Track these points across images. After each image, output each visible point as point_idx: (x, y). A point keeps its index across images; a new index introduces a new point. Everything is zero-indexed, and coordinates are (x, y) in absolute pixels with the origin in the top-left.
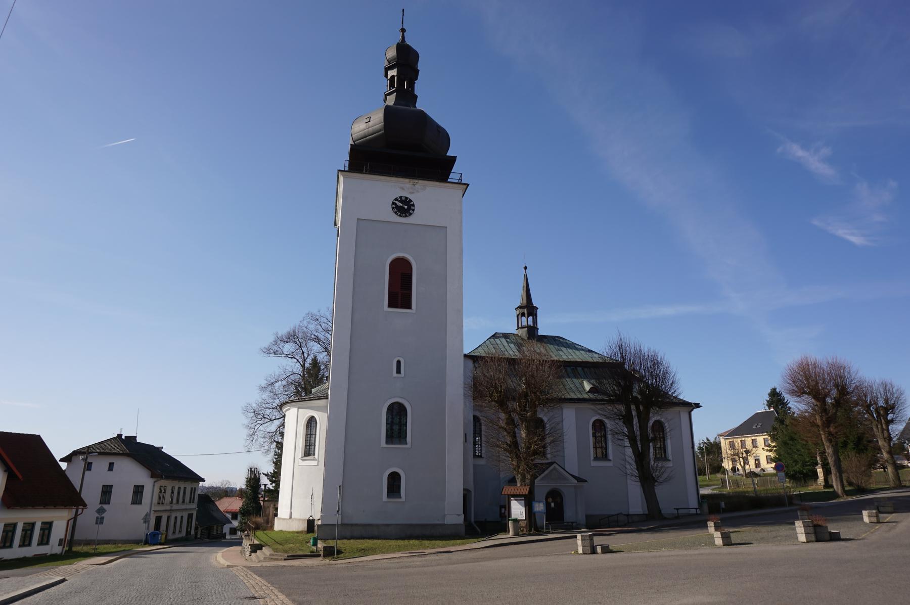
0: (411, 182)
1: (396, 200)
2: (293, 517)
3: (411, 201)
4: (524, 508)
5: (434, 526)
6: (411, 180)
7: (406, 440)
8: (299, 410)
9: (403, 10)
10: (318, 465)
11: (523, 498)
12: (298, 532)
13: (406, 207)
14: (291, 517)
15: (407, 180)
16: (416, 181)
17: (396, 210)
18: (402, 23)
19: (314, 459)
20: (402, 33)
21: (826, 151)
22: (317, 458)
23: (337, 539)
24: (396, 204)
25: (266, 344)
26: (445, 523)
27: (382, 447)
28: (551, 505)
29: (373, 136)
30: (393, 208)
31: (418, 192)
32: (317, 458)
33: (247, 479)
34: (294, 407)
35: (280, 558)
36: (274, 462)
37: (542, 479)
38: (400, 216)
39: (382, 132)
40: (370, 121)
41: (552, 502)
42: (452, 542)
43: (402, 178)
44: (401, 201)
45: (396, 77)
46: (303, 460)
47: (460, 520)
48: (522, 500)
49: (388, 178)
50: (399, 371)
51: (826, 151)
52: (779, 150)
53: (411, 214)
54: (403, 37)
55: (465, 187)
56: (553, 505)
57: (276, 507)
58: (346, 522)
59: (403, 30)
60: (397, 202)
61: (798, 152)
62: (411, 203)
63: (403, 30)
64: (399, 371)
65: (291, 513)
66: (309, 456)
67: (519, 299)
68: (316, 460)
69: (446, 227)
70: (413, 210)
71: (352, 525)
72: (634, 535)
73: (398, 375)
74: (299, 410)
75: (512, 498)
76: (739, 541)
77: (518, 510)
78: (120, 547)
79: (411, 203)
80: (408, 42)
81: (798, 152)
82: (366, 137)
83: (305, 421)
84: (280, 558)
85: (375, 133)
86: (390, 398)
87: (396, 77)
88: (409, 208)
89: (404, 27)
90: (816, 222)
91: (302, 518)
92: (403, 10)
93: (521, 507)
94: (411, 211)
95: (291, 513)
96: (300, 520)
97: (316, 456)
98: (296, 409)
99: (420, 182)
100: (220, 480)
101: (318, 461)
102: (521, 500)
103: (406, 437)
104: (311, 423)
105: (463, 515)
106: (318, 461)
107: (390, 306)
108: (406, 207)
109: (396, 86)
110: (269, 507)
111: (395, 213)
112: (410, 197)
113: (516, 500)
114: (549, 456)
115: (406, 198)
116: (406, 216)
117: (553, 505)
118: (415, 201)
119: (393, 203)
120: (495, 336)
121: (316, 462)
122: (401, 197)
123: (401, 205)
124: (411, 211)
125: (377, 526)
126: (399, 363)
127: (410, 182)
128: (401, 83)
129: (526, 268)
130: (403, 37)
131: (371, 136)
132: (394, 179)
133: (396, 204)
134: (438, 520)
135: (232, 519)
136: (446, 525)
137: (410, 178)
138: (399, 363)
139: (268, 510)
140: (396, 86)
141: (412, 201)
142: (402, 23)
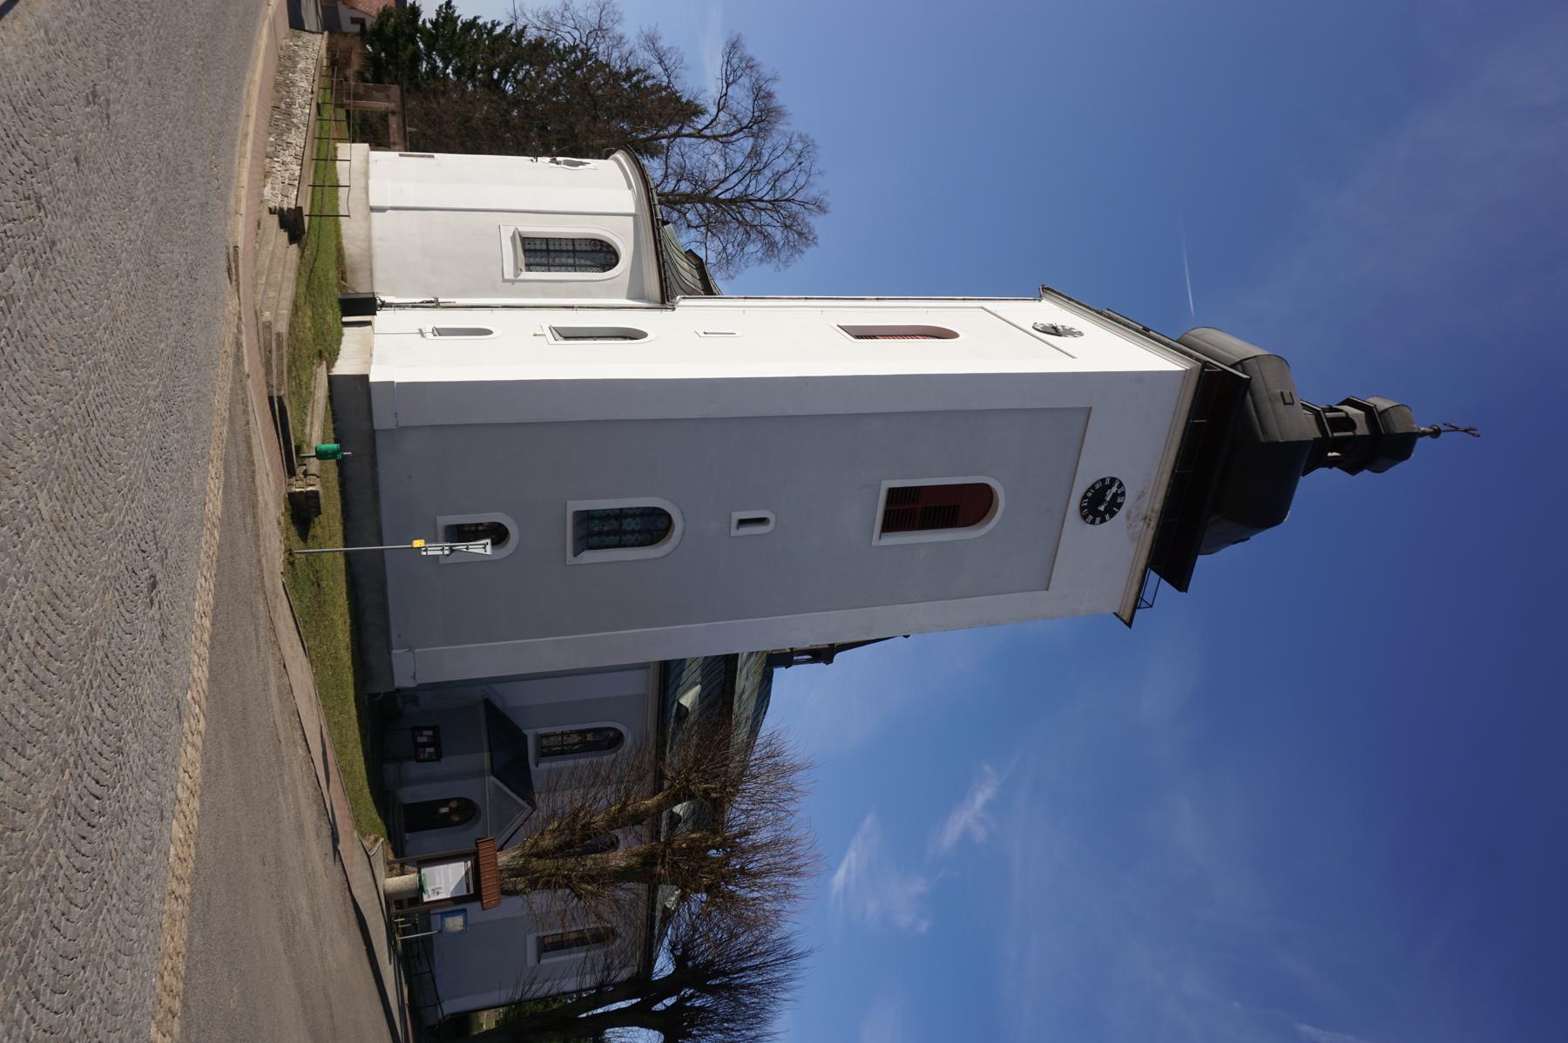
0: (1154, 515)
1: (1121, 485)
2: (375, 215)
3: (1112, 514)
4: (449, 896)
5: (386, 630)
6: (1159, 514)
7: (583, 551)
8: (631, 218)
10: (505, 281)
11: (472, 891)
12: (340, 250)
13: (1102, 508)
14: (373, 209)
15: (1158, 506)
16: (1153, 524)
17: (1097, 486)
19: (517, 270)
20: (1428, 430)
21: (980, 834)
22: (520, 278)
23: (347, 554)
24: (1111, 488)
25: (751, 49)
26: (394, 652)
27: (566, 504)
28: (445, 807)
29: (1254, 414)
30: (1103, 480)
31: (1128, 528)
32: (520, 278)
34: (638, 203)
35: (275, 382)
36: (476, 18)
37: (497, 787)
38: (1085, 497)
39: (1261, 435)
40: (1285, 404)
41: (450, 808)
42: (354, 733)
43: (1166, 497)
44: (1115, 495)
45: (1350, 434)
46: (513, 238)
47: (403, 680)
48: (468, 890)
49: (1169, 468)
51: (980, 834)
52: (987, 768)
53: (1085, 517)
55: (1126, 618)
56: (444, 810)
57: (392, 147)
58: (381, 441)
59: (1436, 433)
60: (1114, 489)
61: (983, 795)
63: (1436, 433)
65: (382, 210)
66: (525, 251)
68: (517, 275)
69: (1047, 589)
70: (1093, 522)
71: (373, 455)
73: (734, 523)
74: (631, 218)
75: (469, 863)
76: (372, 862)
77: (444, 880)
78: (266, 504)
81: (983, 795)
82: (1217, 347)
83: (603, 236)
84: (275, 382)
85: (1259, 419)
86: (684, 533)
87: (1350, 434)
88: (1096, 513)
89: (1442, 434)
90: (869, 821)
91: (376, 243)
93: (452, 888)
94: (1091, 517)
95: (382, 210)
96: (369, 239)
97: (526, 275)
98: (633, 211)
99: (1150, 533)
101: (513, 282)
102: (468, 885)
103: (591, 548)
104: (600, 251)
105: (415, 685)
106: (513, 282)
107: (893, 493)
108: (1102, 508)
109: (1335, 434)
110: (388, 98)
111: (1093, 487)
113: (467, 873)
114: (544, 766)
115: (1119, 506)
116: (1082, 508)
117: (444, 810)
118: (1111, 523)
119: (1113, 480)
121: (512, 277)
125: (377, 512)
126: (762, 521)
127: (1152, 511)
128: (1336, 444)
131: (1257, 422)
132: (1166, 478)
133: (1110, 487)
134: (399, 636)
136: (390, 653)
137: (1161, 512)
139: (381, 95)
140: (1335, 434)
141: (1111, 517)
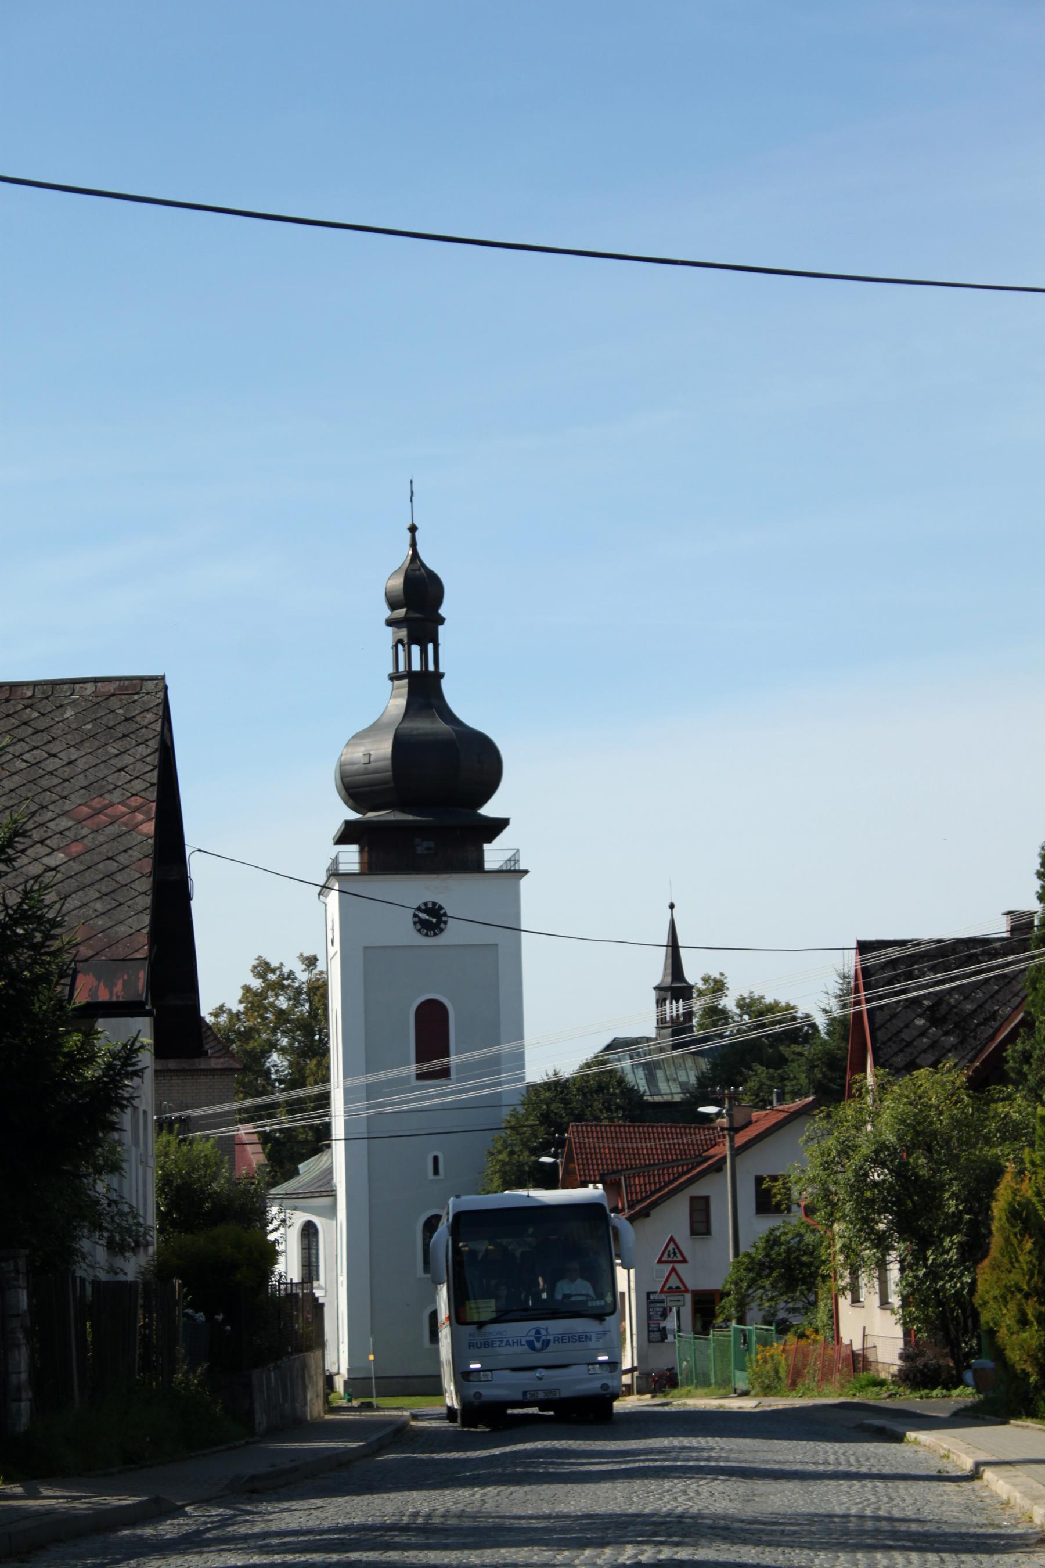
9: (411, 482)
13: (434, 920)
17: (419, 927)
18: (411, 501)
30: (415, 923)
33: (751, 998)
38: (427, 935)
44: (427, 911)
50: (436, 1172)
53: (442, 930)
54: (413, 545)
62: (442, 912)
63: (413, 529)
64: (436, 1172)
67: (657, 971)
72: (410, 1374)
73: (437, 1178)
79: (442, 912)
80: (431, 560)
88: (439, 921)
92: (411, 482)
94: (442, 926)
100: (834, 986)
108: (434, 920)
111: (419, 931)
112: (440, 901)
116: (435, 934)
119: (415, 916)
120: (614, 1045)
122: (425, 904)
123: (427, 917)
124: (442, 926)
126: (436, 1159)
129: (672, 906)
130: (413, 545)
135: (693, 1199)
138: (436, 1159)
142: (411, 501)
